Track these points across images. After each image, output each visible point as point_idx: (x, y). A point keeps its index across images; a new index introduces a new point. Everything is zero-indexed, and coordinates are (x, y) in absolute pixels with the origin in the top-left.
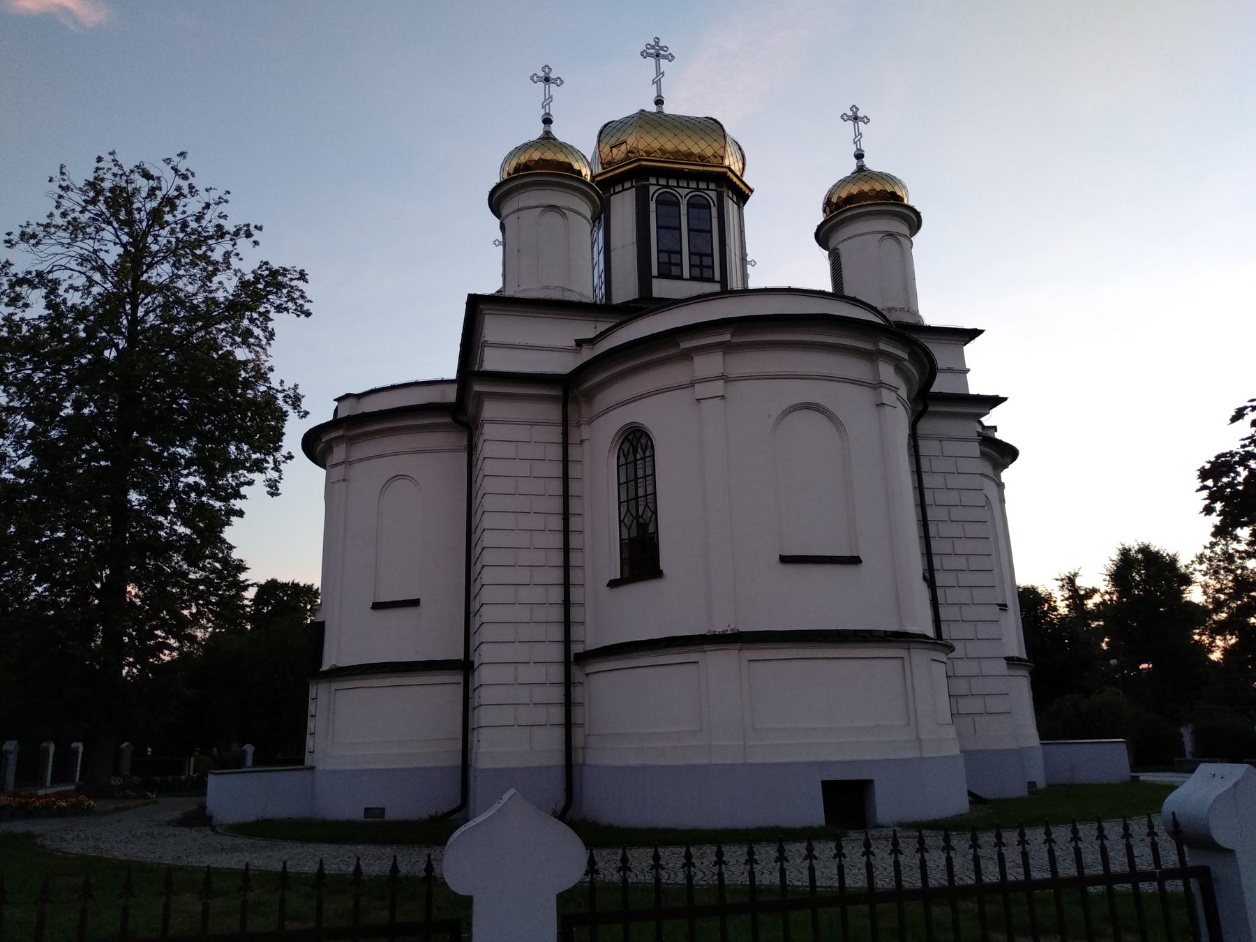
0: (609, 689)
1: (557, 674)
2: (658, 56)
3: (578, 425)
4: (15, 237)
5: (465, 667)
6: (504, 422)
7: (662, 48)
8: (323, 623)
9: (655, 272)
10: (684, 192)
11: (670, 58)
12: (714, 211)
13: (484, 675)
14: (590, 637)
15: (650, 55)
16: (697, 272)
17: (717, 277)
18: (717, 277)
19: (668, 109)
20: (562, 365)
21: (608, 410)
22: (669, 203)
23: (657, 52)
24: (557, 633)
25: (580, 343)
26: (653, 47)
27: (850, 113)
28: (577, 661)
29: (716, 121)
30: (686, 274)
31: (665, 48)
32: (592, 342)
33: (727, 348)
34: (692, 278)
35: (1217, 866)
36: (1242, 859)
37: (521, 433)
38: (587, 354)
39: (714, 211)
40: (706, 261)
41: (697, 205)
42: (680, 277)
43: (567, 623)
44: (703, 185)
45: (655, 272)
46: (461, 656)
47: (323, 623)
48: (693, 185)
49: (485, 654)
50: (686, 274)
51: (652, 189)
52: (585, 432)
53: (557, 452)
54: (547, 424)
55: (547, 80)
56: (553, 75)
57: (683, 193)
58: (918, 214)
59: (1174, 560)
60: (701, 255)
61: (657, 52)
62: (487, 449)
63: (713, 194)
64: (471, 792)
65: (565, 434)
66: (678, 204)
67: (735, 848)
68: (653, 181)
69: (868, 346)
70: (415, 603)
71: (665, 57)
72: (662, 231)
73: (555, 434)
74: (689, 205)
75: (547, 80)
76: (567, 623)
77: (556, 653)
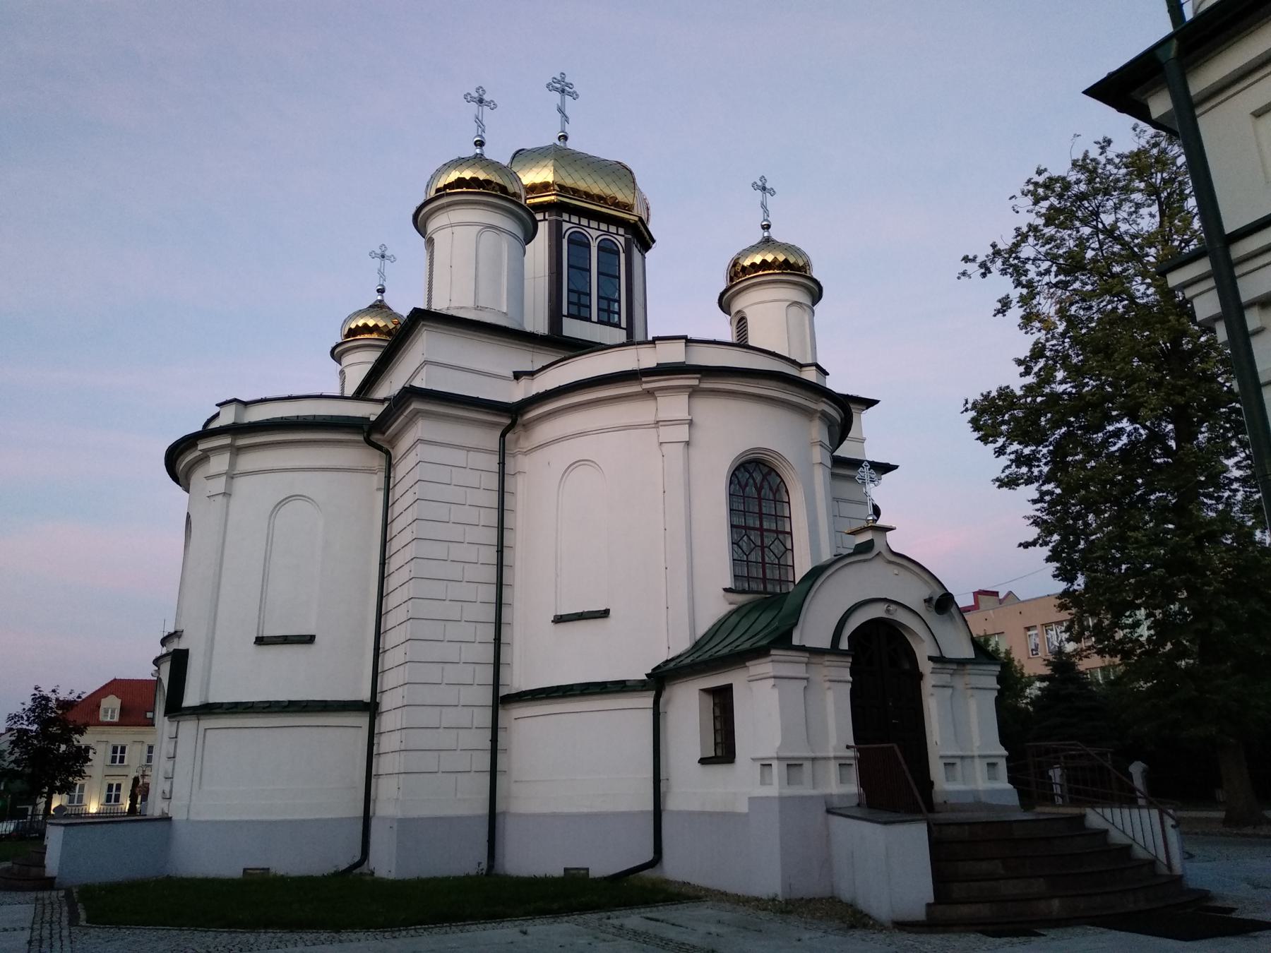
1: (485, 717)
2: (563, 91)
3: (514, 455)
5: (371, 708)
7: (567, 85)
8: (186, 652)
9: (565, 312)
10: (595, 233)
11: (575, 96)
12: (622, 256)
13: (387, 722)
14: (517, 680)
15: (556, 89)
16: (605, 317)
17: (624, 324)
18: (624, 324)
19: (570, 144)
22: (580, 243)
23: (562, 88)
24: (487, 675)
25: (517, 376)
26: (559, 82)
27: (760, 183)
28: (502, 701)
29: (625, 167)
30: (595, 318)
31: (570, 85)
33: (694, 392)
34: (600, 322)
37: (459, 457)
39: (622, 256)
41: (607, 249)
42: (589, 319)
44: (613, 229)
45: (565, 312)
46: (366, 696)
47: (186, 652)
48: (603, 227)
49: (386, 702)
50: (595, 318)
51: (566, 226)
55: (481, 101)
56: (486, 97)
57: (594, 233)
58: (821, 289)
61: (562, 88)
62: (400, 471)
63: (622, 240)
65: (502, 464)
66: (588, 246)
68: (565, 216)
70: (309, 640)
71: (570, 94)
72: (572, 270)
74: (599, 248)
75: (481, 101)
77: (489, 700)
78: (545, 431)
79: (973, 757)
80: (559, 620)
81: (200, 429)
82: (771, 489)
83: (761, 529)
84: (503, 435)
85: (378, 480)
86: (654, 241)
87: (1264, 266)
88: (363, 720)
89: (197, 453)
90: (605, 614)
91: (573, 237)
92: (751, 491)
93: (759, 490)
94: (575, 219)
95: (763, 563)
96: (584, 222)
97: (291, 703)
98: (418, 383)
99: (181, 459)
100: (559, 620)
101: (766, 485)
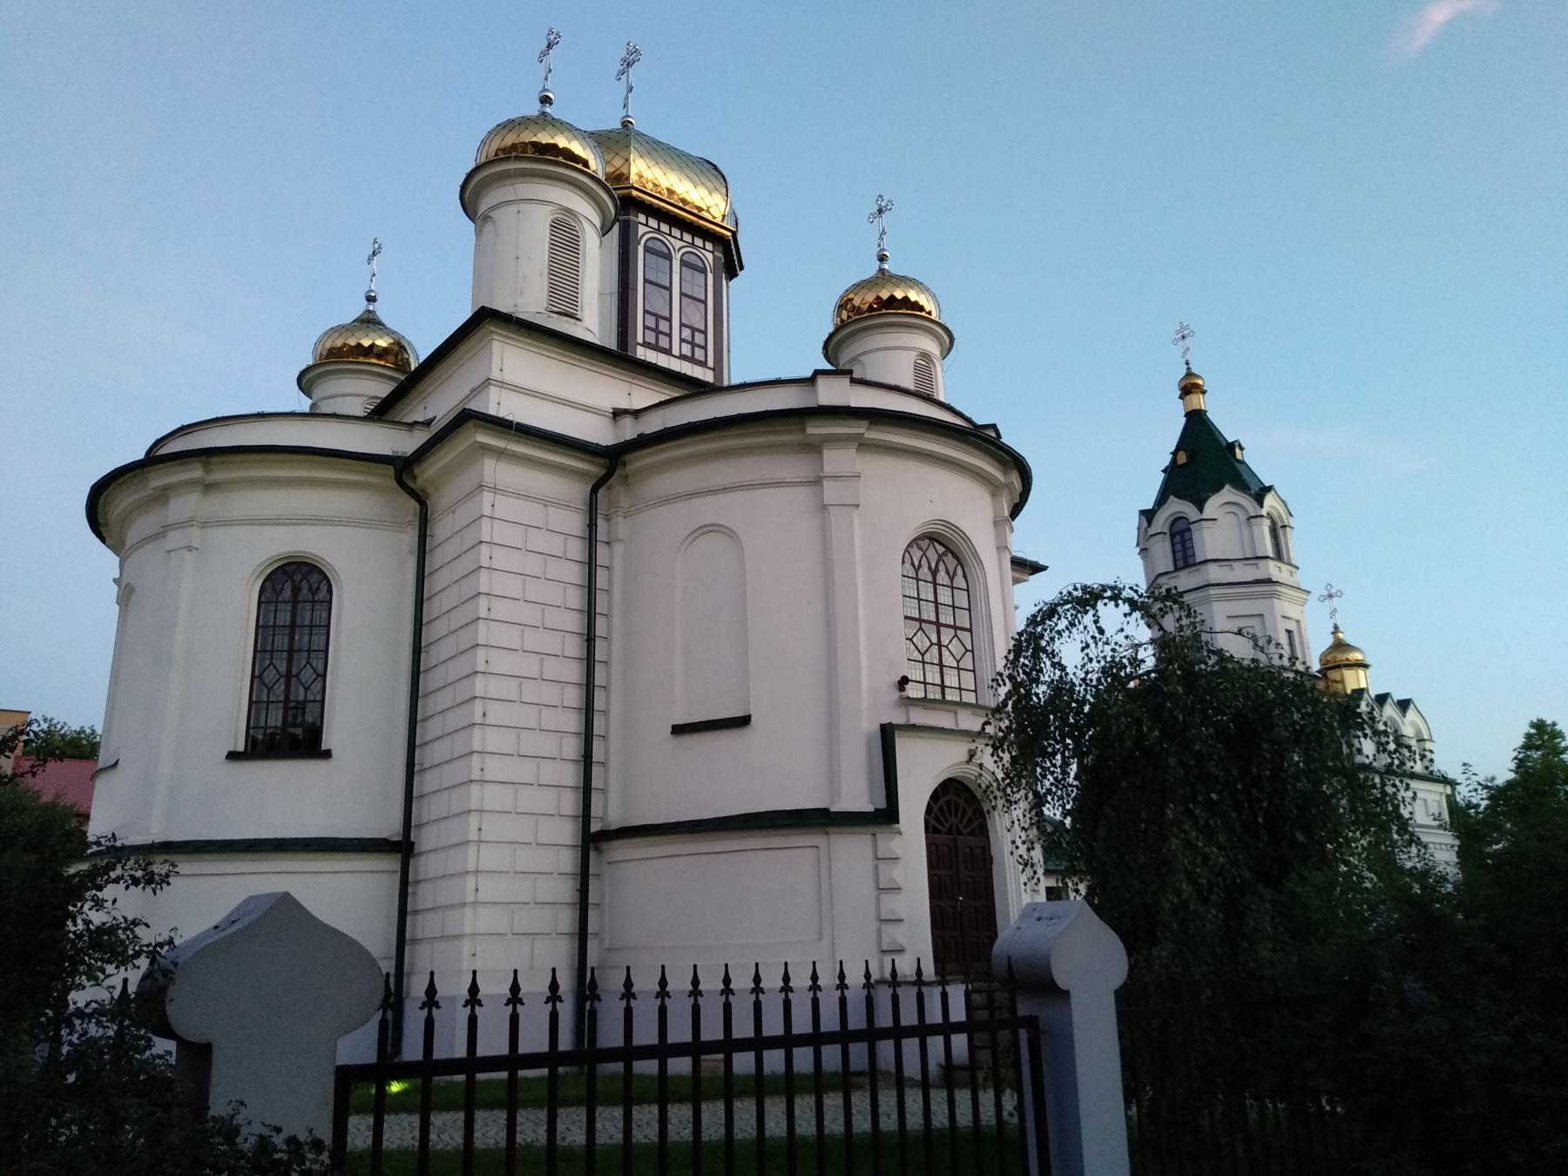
0: (636, 875)
1: (567, 861)
4: (1198, 401)
6: (518, 496)
9: (640, 340)
10: (679, 244)
14: (611, 812)
16: (686, 349)
17: (710, 363)
18: (710, 363)
20: (600, 433)
21: (668, 500)
24: (570, 803)
25: (617, 414)
28: (593, 840)
30: (676, 351)
32: (636, 414)
35: (1046, 1012)
36: (1076, 1001)
37: (532, 513)
38: (629, 430)
40: (699, 338)
43: (586, 789)
45: (640, 340)
51: (642, 229)
52: (622, 527)
53: (577, 549)
54: (566, 506)
59: (82, 731)
60: (658, 317)
64: (599, 1030)
65: (592, 525)
66: (669, 258)
67: (646, 1108)
68: (642, 218)
69: (1000, 476)
72: (687, 272)
73: (574, 522)
76: (586, 789)
77: (567, 832)
78: (661, 484)
79: (464, 904)
80: (679, 730)
81: (141, 456)
82: (947, 572)
83: (938, 624)
84: (594, 490)
85: (410, 537)
86: (742, 268)
87: (726, 489)
88: (392, 863)
89: (148, 492)
90: (743, 721)
91: (650, 244)
92: (925, 572)
93: (934, 573)
94: (653, 223)
95: (941, 665)
96: (665, 228)
97: (187, 843)
98: (475, 406)
99: (106, 505)
100: (679, 730)
101: (942, 567)
